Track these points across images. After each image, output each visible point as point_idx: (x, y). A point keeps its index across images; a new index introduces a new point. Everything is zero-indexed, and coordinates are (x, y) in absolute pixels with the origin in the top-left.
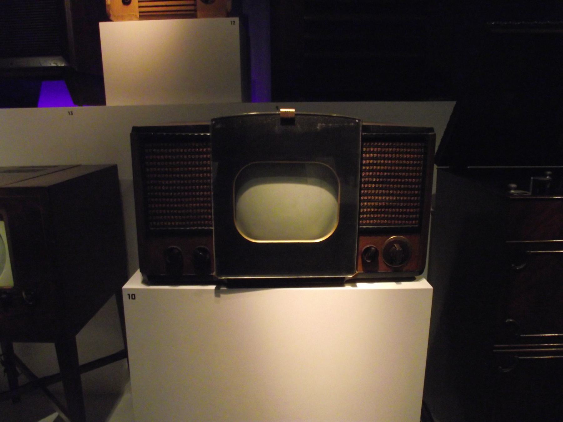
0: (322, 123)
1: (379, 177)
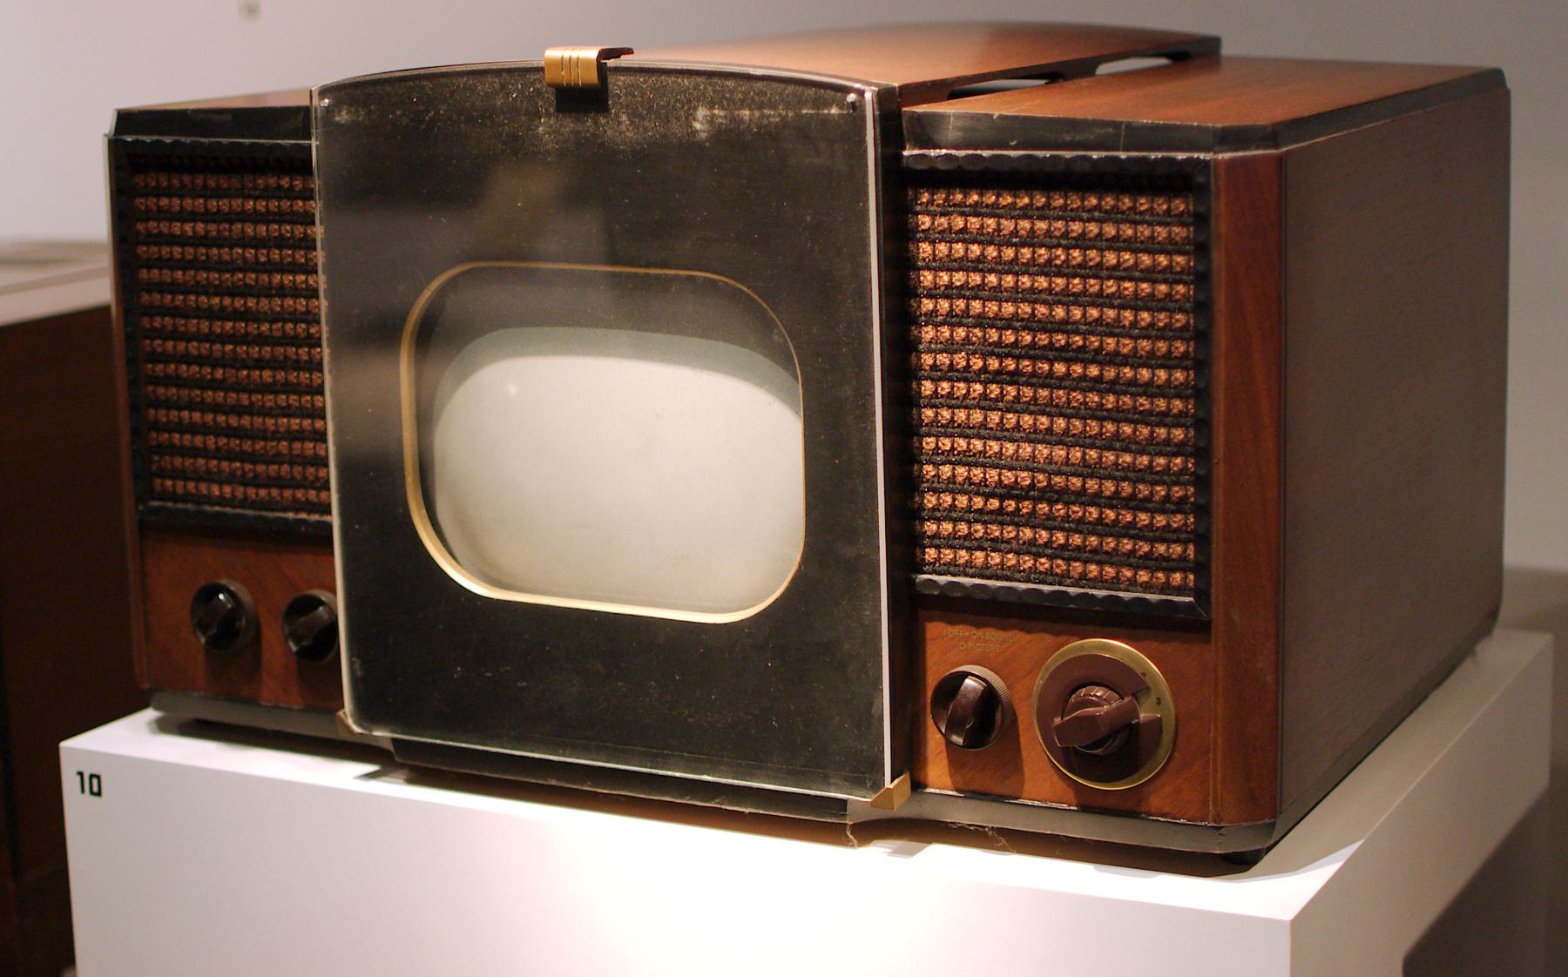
0: (712, 108)
1: (1000, 350)
